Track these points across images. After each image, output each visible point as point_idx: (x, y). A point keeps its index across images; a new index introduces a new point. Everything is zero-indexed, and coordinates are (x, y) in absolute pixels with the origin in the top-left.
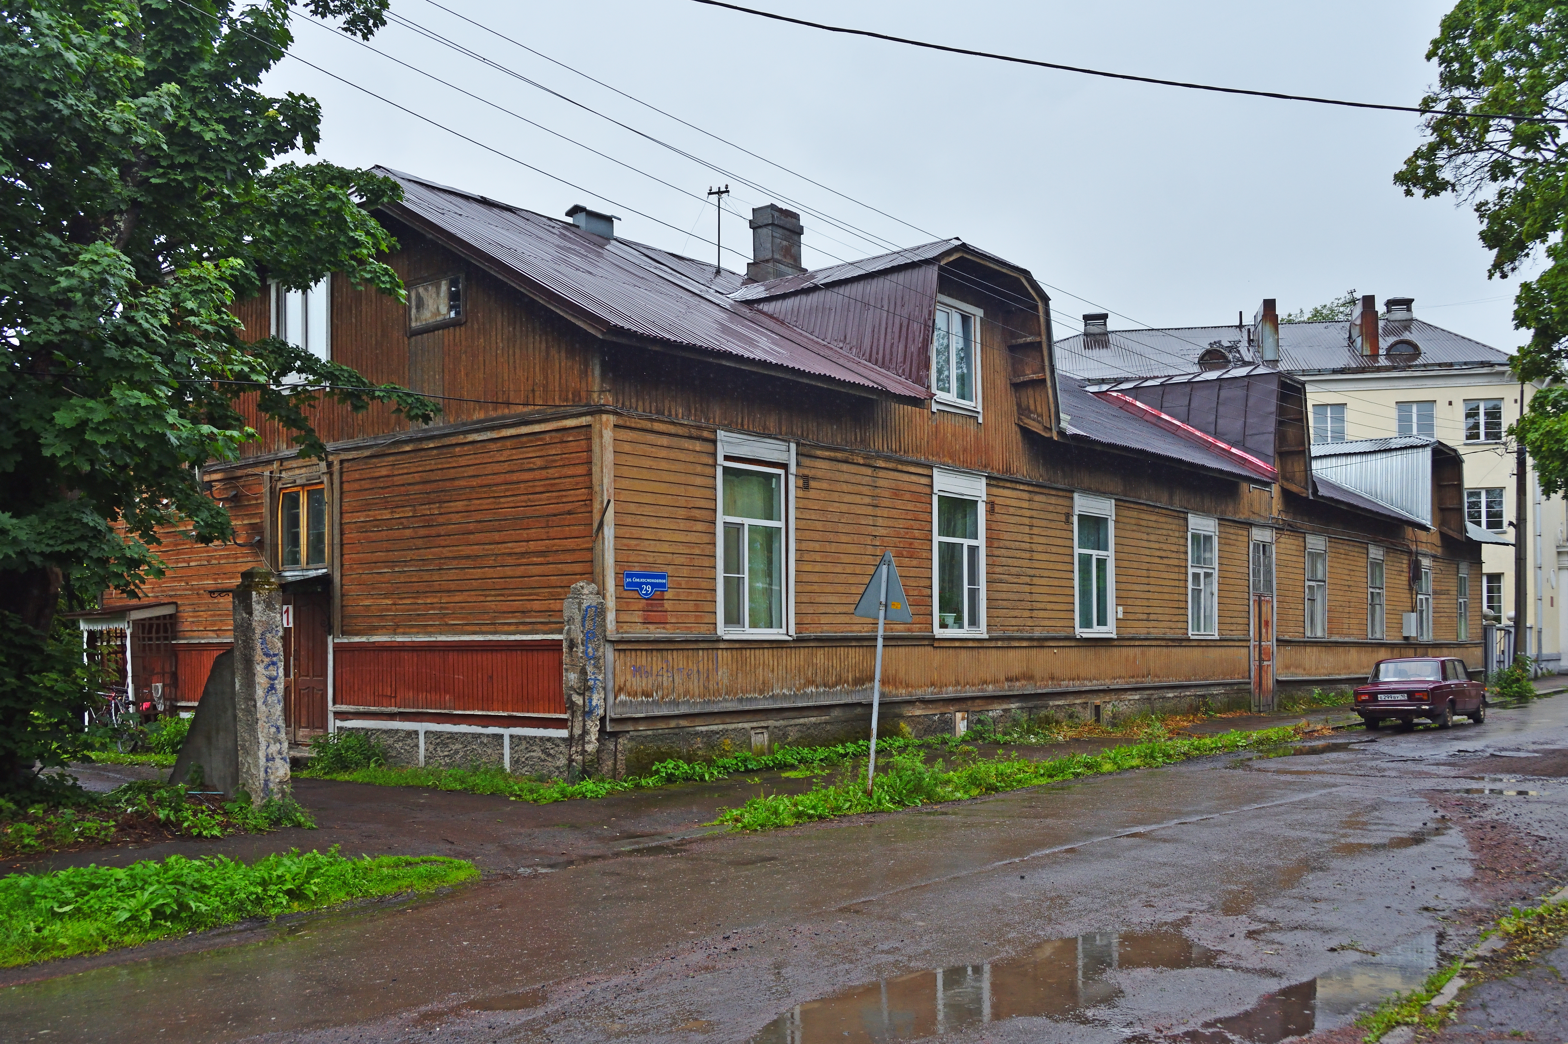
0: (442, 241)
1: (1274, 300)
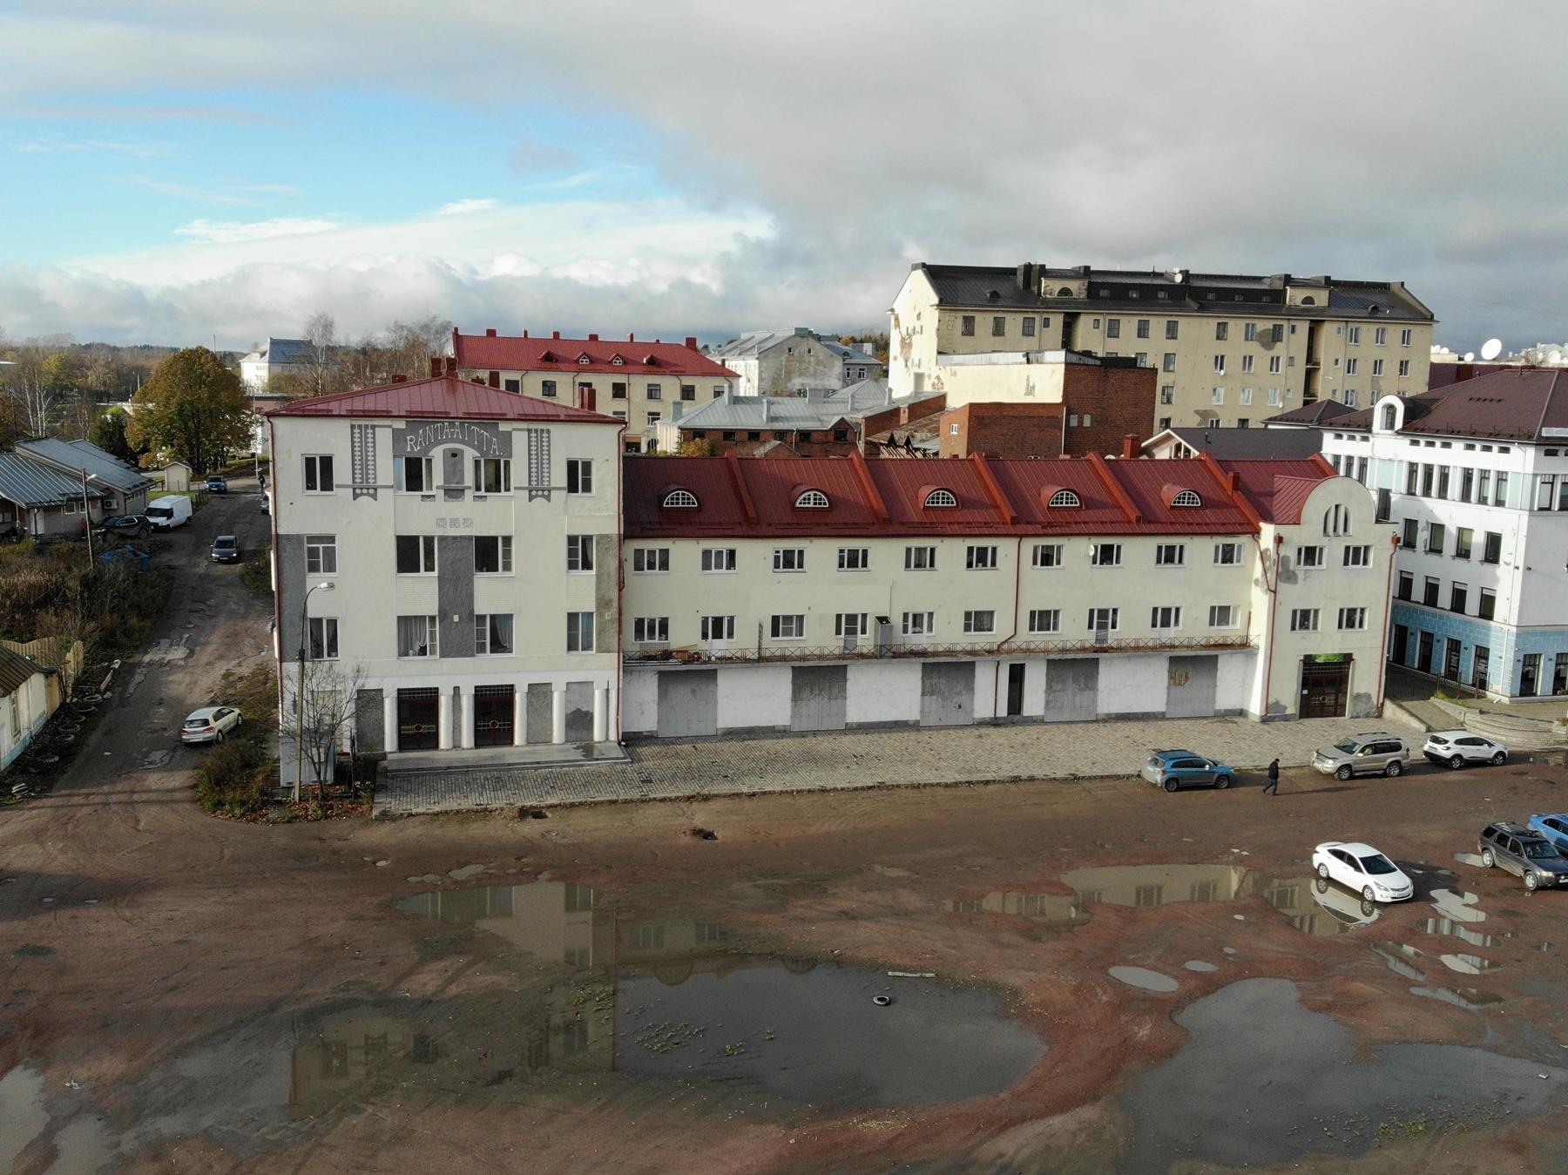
0: (818, 530)
1: (399, 618)
